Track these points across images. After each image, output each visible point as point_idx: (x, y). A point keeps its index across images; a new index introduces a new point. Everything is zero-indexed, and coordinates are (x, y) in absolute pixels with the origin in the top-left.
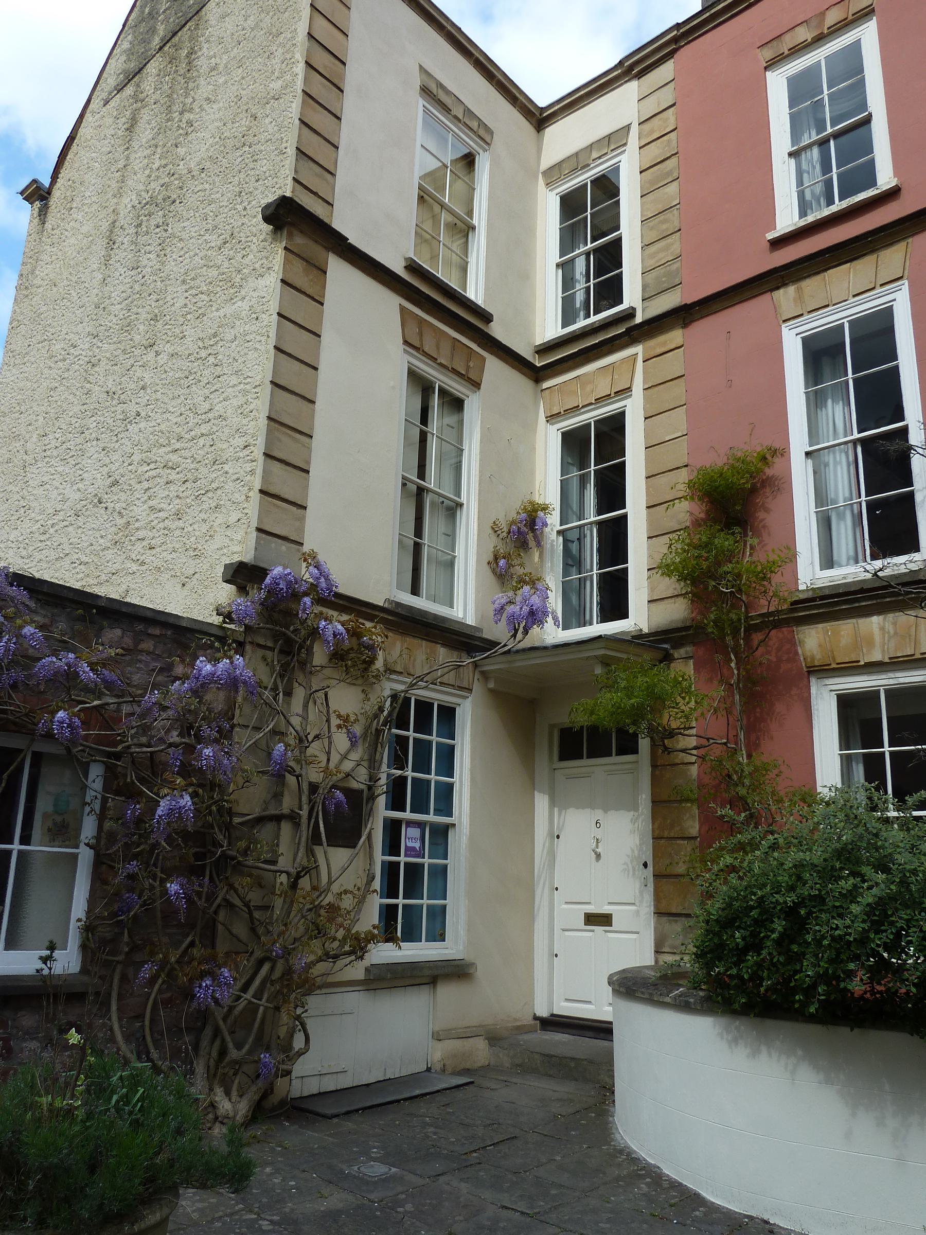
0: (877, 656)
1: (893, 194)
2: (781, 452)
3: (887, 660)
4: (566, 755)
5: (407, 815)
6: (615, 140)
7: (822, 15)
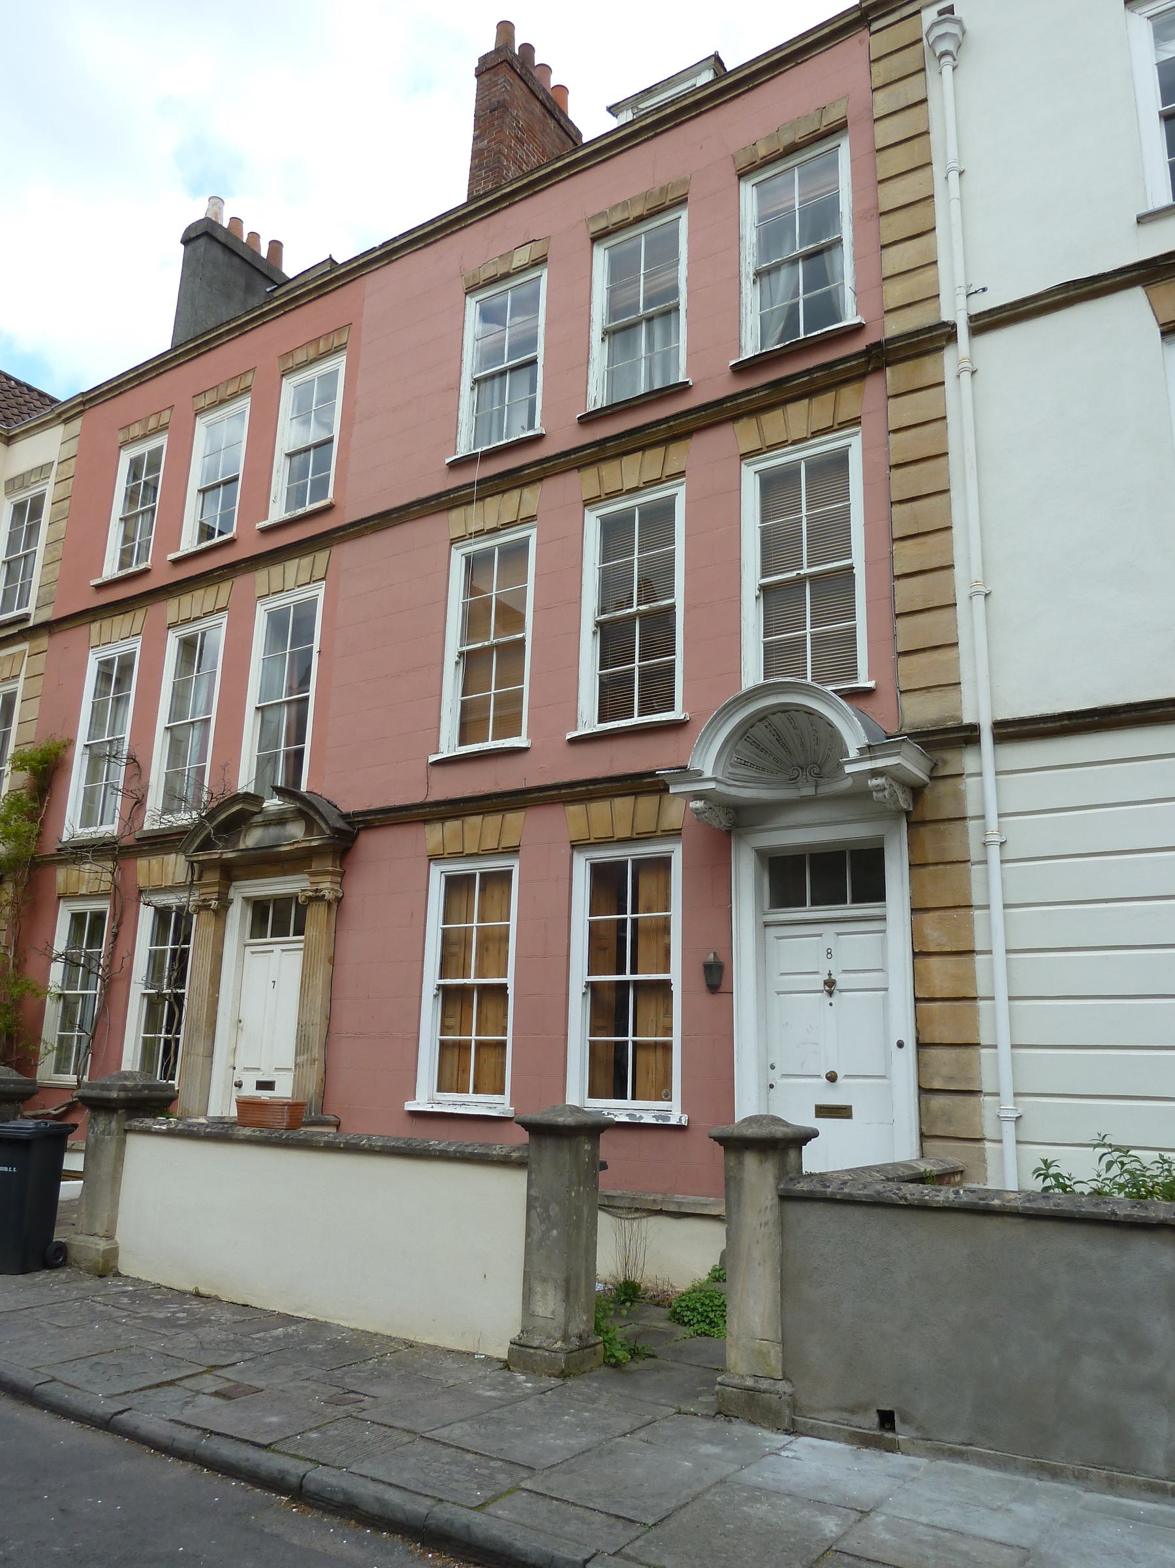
0: (83, 891)
1: (858, 329)
2: (70, 743)
3: (635, 836)
4: (258, 929)
5: (628, 977)
6: (42, 471)
7: (510, 254)
